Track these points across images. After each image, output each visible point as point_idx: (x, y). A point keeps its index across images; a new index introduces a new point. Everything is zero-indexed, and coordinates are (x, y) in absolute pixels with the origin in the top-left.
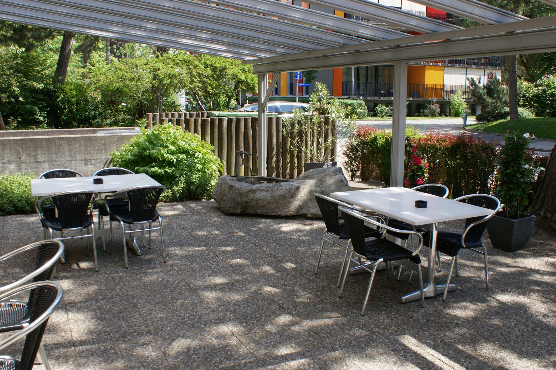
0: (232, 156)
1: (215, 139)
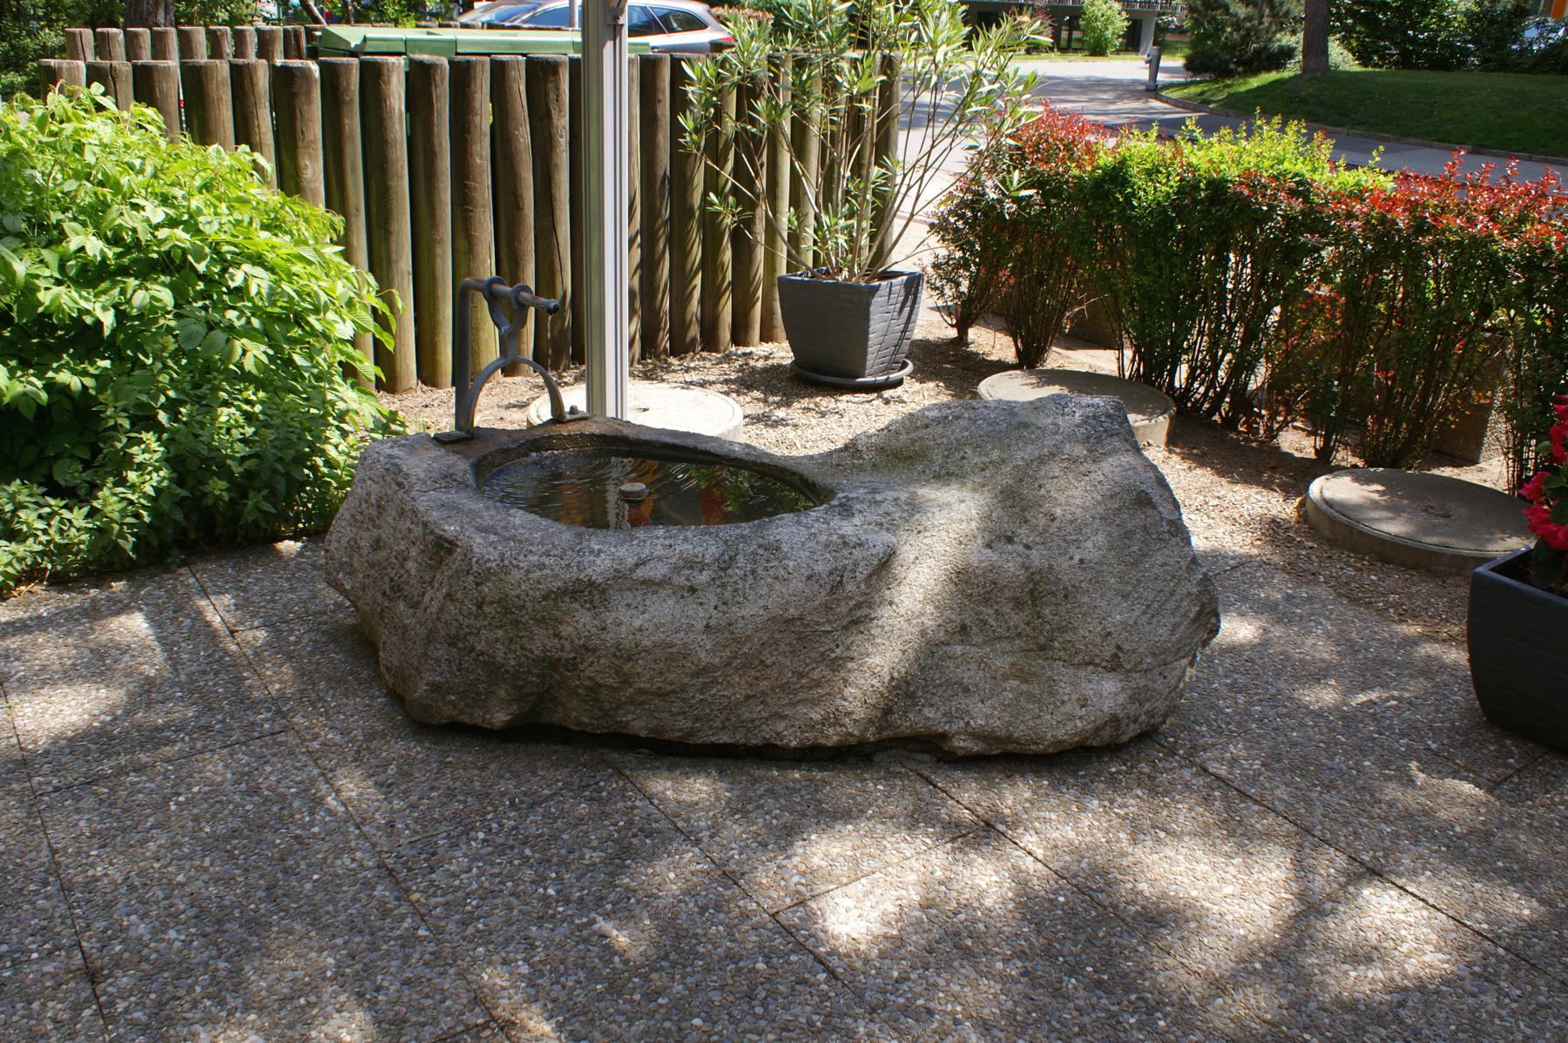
0: (439, 251)
1: (348, 166)
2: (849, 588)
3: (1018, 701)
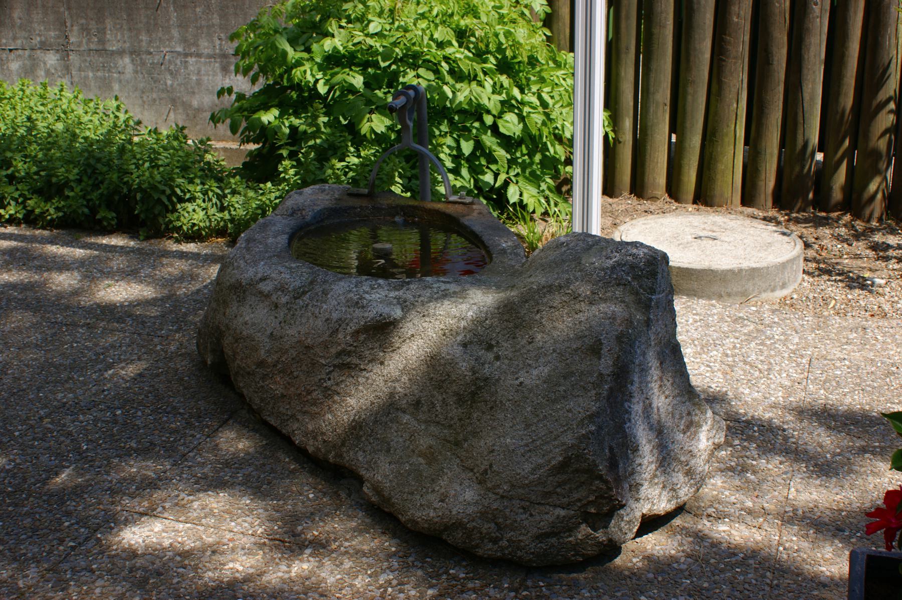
2: (339, 336)
3: (409, 475)
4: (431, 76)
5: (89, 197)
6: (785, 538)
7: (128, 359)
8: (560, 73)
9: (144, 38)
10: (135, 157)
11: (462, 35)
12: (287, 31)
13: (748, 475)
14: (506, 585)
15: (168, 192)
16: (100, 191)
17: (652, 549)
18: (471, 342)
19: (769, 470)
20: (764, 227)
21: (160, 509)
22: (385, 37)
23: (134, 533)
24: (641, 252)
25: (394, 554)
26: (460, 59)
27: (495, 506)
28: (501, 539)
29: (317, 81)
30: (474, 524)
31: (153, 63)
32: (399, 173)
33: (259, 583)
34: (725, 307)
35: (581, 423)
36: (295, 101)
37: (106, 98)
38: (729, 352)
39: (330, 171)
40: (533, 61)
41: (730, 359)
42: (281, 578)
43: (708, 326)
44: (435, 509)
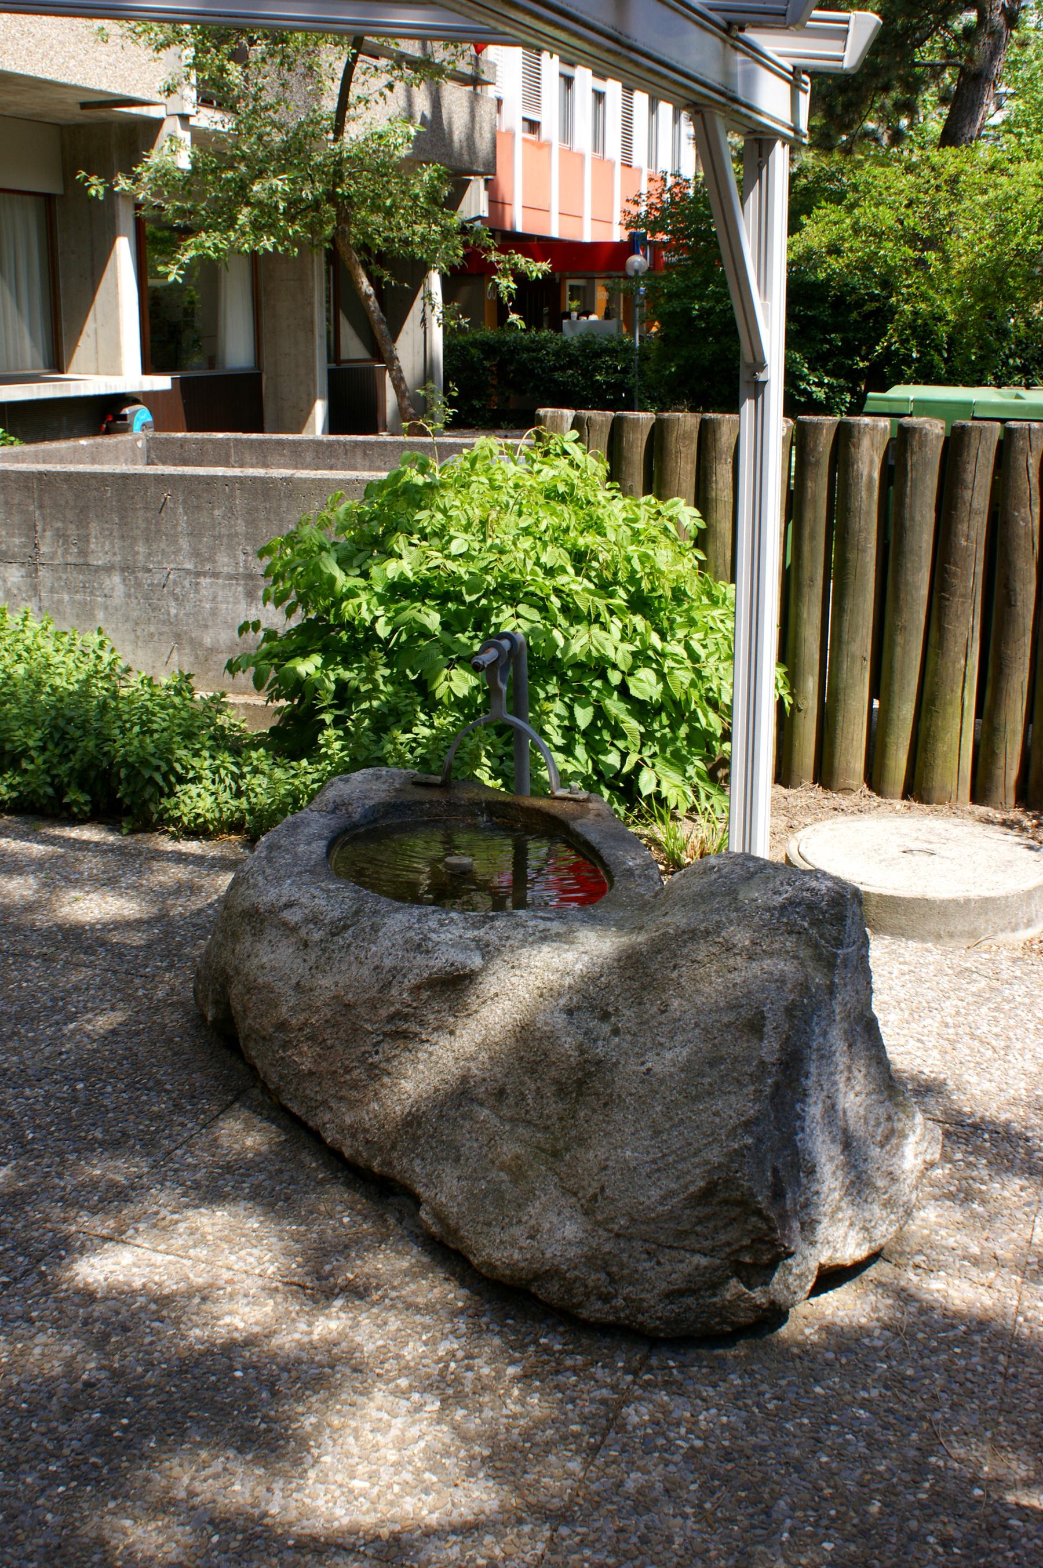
3: (485, 1197)
4: (535, 615)
5: (55, 772)
6: (1026, 1304)
7: (96, 1008)
8: (717, 613)
9: (141, 550)
10: (119, 717)
11: (580, 558)
12: (338, 547)
13: (975, 1206)
14: (620, 1364)
15: (164, 768)
16: (70, 764)
17: (833, 1315)
18: (579, 1008)
19: (1004, 1198)
20: (1003, 837)
21: (131, 1232)
22: (472, 558)
23: (92, 1266)
24: (823, 886)
25: (461, 1312)
26: (577, 593)
27: (606, 1248)
28: (615, 1296)
29: (376, 619)
30: (576, 1273)
31: (152, 584)
32: (487, 751)
33: (266, 1349)
34: (944, 954)
35: (732, 1134)
36: (345, 645)
37: (85, 631)
38: (949, 1020)
39: (389, 747)
40: (679, 595)
41: (952, 1031)
42: (298, 1341)
43: (920, 981)
44: (521, 1248)
